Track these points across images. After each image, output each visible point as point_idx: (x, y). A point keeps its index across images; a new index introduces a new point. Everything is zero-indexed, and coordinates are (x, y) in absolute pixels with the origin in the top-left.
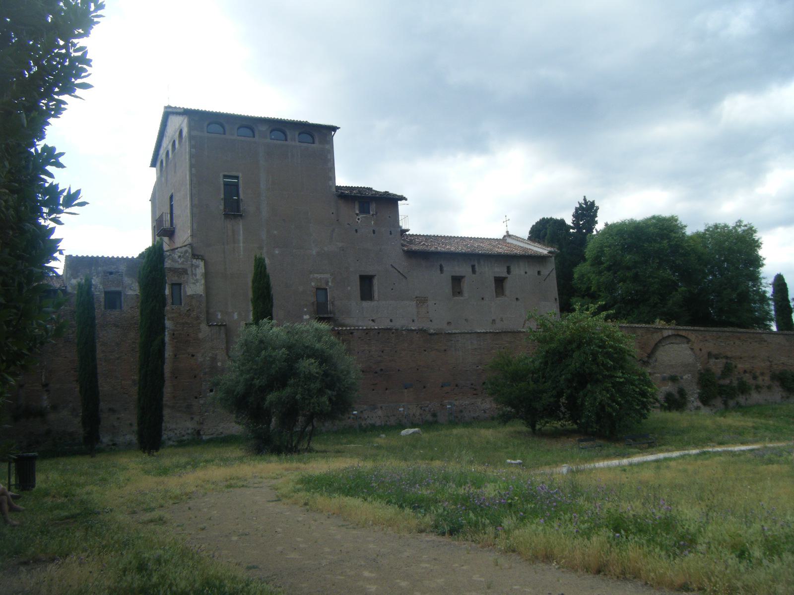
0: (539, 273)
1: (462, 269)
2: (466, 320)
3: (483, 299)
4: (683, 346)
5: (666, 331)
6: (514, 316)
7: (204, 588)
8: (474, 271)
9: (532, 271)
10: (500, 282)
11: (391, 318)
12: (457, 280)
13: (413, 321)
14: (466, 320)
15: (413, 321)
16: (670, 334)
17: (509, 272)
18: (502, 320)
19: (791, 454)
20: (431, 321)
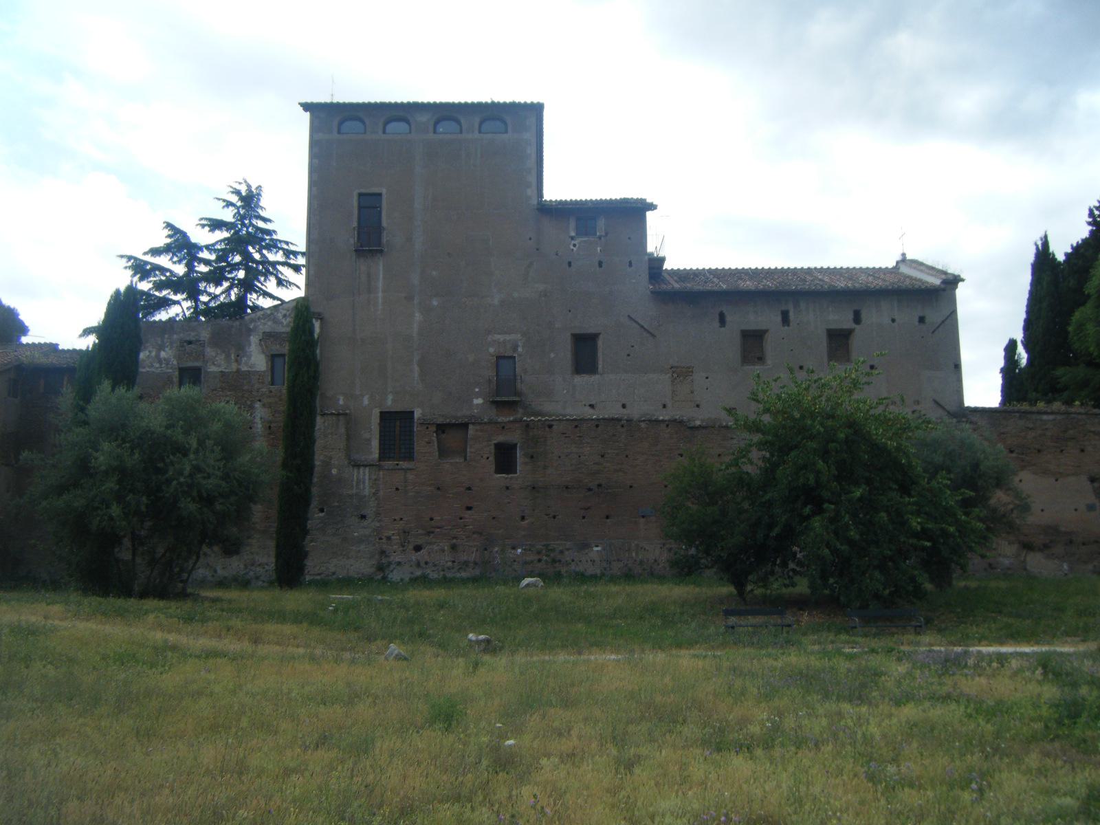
0: (922, 320)
13: (664, 406)
15: (664, 406)
17: (857, 319)
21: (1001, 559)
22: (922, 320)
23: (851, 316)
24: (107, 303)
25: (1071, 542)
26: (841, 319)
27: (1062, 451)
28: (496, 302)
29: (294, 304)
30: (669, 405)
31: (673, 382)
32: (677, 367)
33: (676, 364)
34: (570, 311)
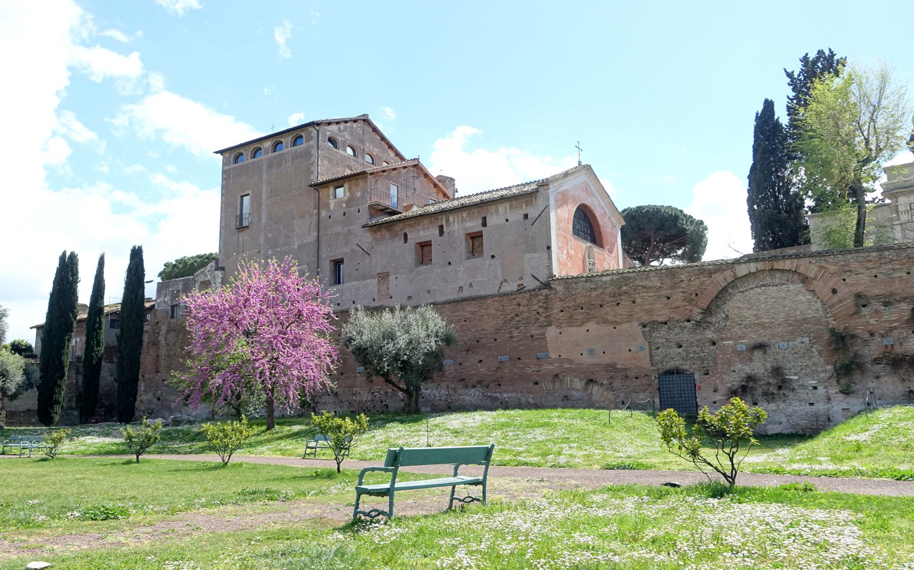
0: (526, 216)
1: (428, 233)
2: (429, 292)
3: (450, 263)
4: (791, 287)
5: (743, 266)
6: (486, 279)
7: (516, 377)
8: (441, 233)
9: (516, 216)
10: (475, 238)
11: (353, 299)
12: (425, 246)
13: (374, 300)
14: (429, 292)
15: (374, 300)
16: (753, 270)
17: (484, 224)
18: (471, 285)
19: (827, 53)
20: (391, 297)
21: (573, 392)
22: (526, 216)
23: (480, 222)
24: (640, 205)
25: (627, 377)
26: (474, 225)
27: (618, 304)
28: (296, 247)
29: (576, 219)
30: (376, 300)
31: (379, 283)
32: (380, 274)
33: (381, 272)
34: (496, 340)
